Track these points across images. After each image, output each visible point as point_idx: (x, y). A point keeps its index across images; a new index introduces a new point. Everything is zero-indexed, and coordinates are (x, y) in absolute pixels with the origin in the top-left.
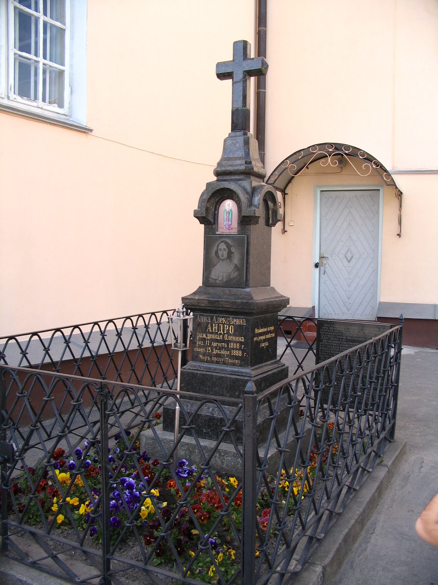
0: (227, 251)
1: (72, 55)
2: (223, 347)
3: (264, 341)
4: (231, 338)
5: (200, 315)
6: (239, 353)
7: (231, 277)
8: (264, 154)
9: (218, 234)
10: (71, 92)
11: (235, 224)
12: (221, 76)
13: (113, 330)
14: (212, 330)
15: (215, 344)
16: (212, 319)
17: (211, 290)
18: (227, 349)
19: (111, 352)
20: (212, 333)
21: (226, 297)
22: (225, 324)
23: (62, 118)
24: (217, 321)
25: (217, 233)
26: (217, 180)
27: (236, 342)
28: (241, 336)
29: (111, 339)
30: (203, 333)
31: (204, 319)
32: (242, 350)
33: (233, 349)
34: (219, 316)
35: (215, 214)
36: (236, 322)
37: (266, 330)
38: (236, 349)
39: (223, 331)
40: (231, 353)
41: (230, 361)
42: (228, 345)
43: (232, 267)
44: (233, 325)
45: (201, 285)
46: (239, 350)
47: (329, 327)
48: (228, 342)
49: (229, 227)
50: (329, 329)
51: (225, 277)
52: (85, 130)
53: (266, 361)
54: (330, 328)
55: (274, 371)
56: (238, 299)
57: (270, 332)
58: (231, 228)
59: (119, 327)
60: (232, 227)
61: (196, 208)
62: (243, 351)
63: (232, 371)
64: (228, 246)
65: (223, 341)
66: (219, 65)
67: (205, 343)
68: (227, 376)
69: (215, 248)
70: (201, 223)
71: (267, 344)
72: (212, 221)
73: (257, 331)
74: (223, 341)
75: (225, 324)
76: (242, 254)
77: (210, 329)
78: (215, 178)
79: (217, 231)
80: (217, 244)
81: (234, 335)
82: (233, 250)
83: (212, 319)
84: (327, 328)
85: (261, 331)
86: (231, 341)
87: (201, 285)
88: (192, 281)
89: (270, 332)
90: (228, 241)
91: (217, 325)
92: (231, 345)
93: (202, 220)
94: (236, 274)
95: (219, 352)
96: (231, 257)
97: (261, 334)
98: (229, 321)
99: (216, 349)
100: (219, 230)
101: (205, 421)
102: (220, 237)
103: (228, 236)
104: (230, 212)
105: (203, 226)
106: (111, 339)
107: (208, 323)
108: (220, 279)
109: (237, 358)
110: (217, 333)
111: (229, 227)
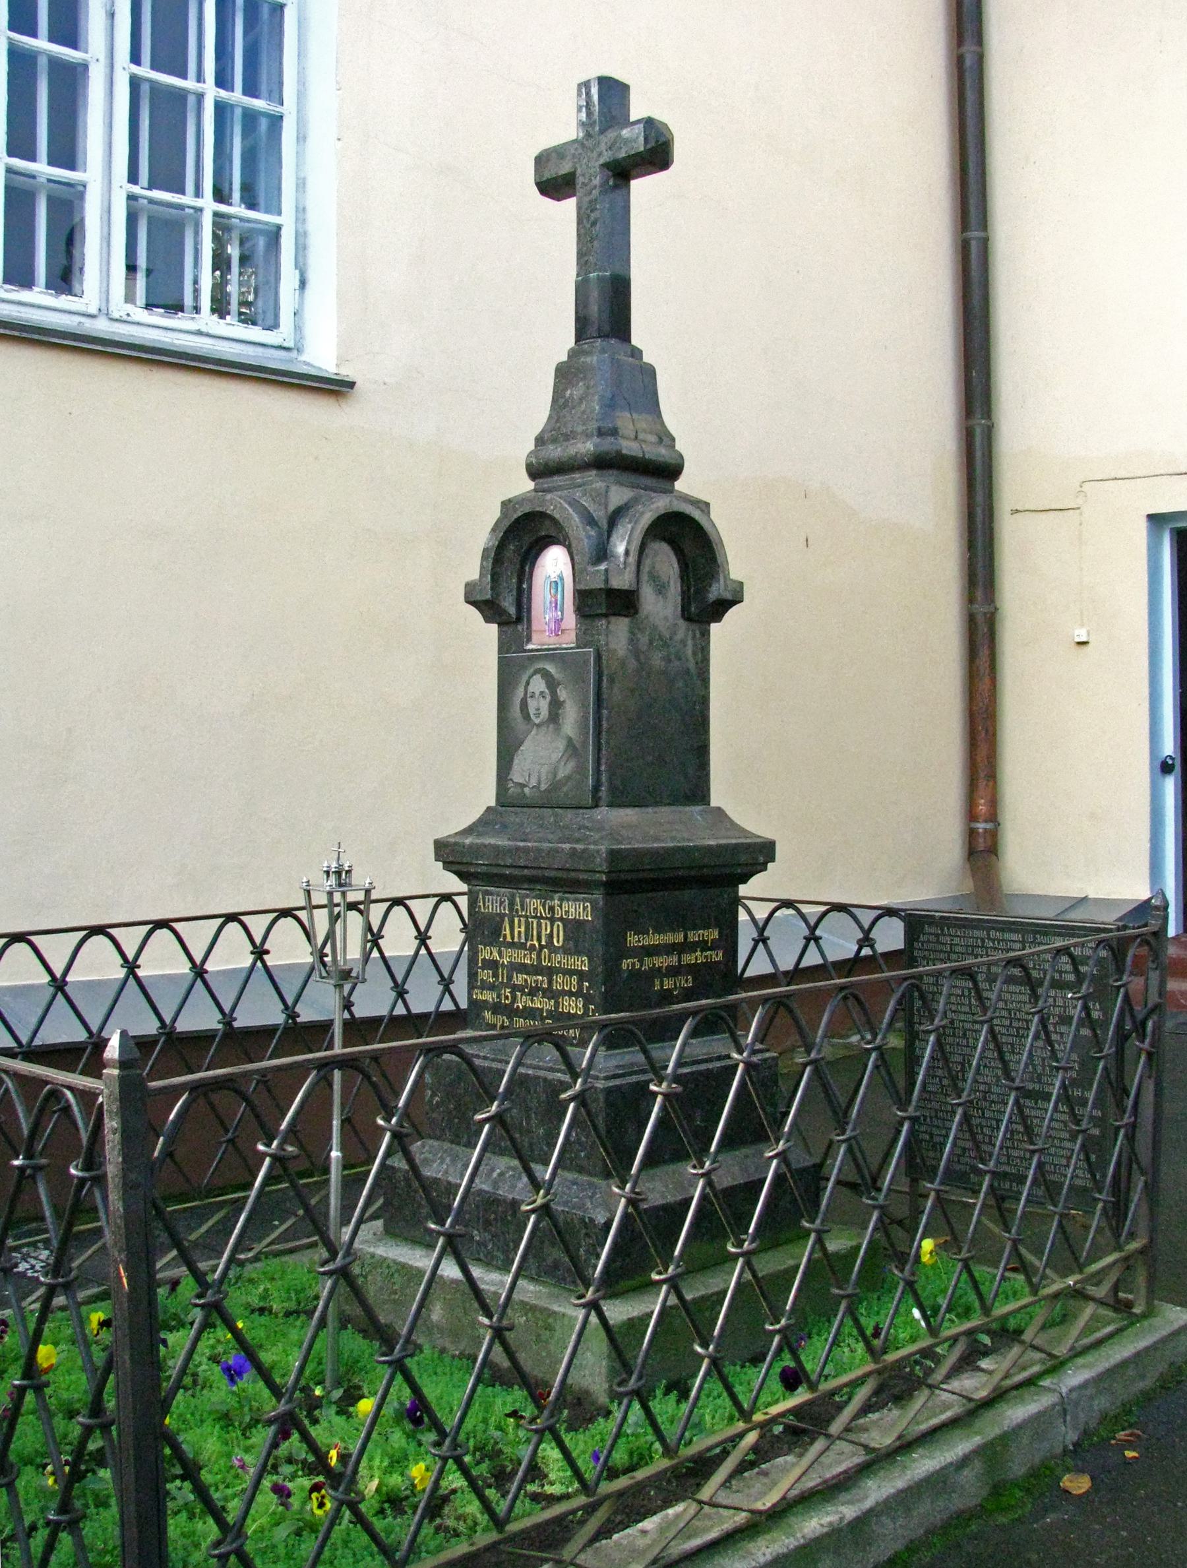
0: (548, 698)
1: (301, 185)
2: (538, 989)
3: (674, 971)
4: (559, 960)
7: (561, 775)
10: (303, 283)
11: (570, 620)
12: (554, 186)
14: (513, 938)
15: (519, 979)
16: (512, 904)
17: (513, 817)
18: (550, 993)
20: (512, 945)
21: (543, 839)
22: (542, 917)
23: (275, 360)
24: (523, 910)
25: (530, 647)
26: (535, 490)
27: (571, 973)
28: (578, 953)
30: (491, 945)
31: (494, 903)
33: (564, 993)
34: (527, 896)
35: (520, 591)
36: (567, 912)
37: (679, 938)
38: (570, 994)
39: (539, 939)
40: (557, 1003)
42: (550, 982)
43: (561, 745)
44: (561, 919)
45: (493, 803)
46: (578, 994)
47: (937, 935)
48: (550, 972)
49: (558, 629)
50: (938, 942)
51: (543, 777)
52: (336, 388)
54: (941, 939)
55: (710, 1066)
56: (568, 840)
57: (703, 945)
58: (563, 631)
61: (475, 575)
62: (588, 999)
64: (552, 684)
65: (537, 970)
66: (541, 160)
67: (495, 975)
68: (541, 1073)
69: (520, 692)
72: (512, 610)
74: (537, 970)
75: (542, 917)
76: (584, 706)
77: (508, 932)
78: (530, 485)
79: (529, 639)
80: (525, 678)
81: (566, 951)
82: (562, 694)
83: (512, 904)
84: (932, 938)
87: (493, 803)
89: (703, 945)
90: (551, 668)
93: (489, 608)
94: (571, 765)
95: (529, 1004)
96: (557, 715)
97: (651, 951)
98: (552, 909)
99: (523, 993)
100: (535, 637)
101: (477, 1207)
102: (538, 658)
103: (551, 655)
105: (495, 627)
107: (502, 916)
108: (533, 783)
110: (522, 946)
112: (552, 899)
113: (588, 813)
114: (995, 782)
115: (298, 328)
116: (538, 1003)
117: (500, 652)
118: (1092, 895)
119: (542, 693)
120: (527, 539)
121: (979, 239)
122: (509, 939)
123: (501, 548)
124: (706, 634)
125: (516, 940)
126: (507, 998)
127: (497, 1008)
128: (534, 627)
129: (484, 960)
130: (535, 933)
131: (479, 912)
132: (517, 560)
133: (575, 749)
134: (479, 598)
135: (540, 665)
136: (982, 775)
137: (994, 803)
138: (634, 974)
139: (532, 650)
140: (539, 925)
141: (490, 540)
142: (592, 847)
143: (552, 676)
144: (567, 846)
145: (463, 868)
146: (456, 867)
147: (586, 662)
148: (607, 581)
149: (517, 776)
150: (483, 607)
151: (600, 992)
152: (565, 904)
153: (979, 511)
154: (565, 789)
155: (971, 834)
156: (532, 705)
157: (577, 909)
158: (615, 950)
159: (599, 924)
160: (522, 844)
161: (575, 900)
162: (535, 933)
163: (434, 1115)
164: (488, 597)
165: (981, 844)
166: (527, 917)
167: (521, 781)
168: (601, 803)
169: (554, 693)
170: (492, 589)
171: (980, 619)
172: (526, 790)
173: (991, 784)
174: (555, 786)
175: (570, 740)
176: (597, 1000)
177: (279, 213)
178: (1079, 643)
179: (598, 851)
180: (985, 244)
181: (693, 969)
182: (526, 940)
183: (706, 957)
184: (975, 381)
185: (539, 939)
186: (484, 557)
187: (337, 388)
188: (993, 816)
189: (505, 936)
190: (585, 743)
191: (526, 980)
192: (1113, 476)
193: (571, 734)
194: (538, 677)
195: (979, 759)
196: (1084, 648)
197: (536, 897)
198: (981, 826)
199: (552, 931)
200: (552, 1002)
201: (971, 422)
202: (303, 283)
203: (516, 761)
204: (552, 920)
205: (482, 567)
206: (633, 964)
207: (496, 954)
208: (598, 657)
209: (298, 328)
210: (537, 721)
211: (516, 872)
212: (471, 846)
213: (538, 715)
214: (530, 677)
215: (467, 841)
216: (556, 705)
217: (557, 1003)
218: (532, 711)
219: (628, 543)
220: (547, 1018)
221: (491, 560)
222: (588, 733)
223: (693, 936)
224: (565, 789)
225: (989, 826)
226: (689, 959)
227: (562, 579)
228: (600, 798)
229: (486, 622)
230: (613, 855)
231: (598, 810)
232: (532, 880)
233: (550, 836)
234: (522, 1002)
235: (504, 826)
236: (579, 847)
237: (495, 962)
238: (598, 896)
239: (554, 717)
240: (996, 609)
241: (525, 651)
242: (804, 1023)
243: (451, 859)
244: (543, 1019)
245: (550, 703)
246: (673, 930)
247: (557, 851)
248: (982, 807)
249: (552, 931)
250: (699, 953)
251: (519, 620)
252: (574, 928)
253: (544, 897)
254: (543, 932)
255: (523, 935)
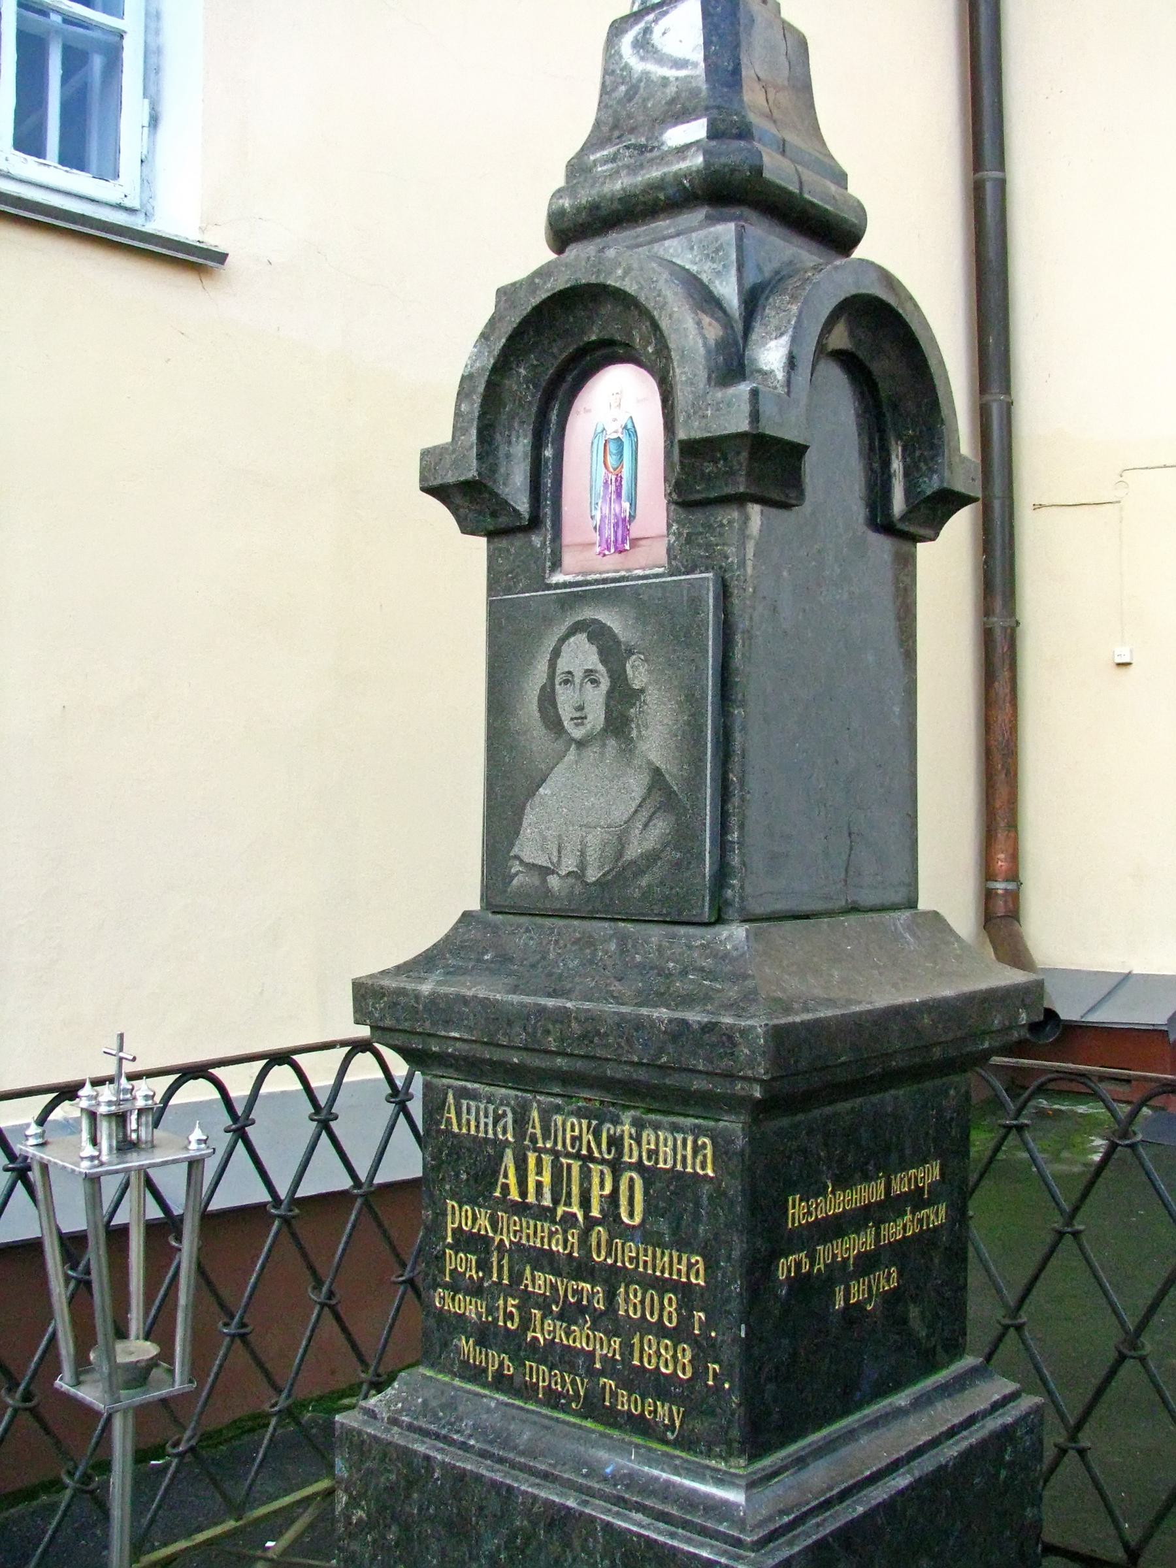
0: (605, 684)
3: (867, 1263)
4: (629, 1253)
5: (462, 1094)
6: (669, 1359)
7: (633, 851)
8: (1010, 404)
9: (557, 586)
10: (154, 121)
11: (653, 512)
13: (379, 1080)
14: (523, 1194)
15: (540, 1282)
16: (521, 1121)
17: (522, 937)
18: (607, 1320)
19: (283, 1193)
20: (521, 1209)
21: (600, 986)
22: (590, 1158)
24: (546, 1137)
25: (558, 578)
27: (662, 1286)
28: (683, 1244)
29: (282, 1139)
30: (473, 1202)
31: (477, 1116)
32: (695, 1343)
33: (643, 1327)
34: (558, 1109)
38: (661, 1331)
39: (585, 1203)
40: (627, 1348)
41: (625, 1403)
42: (611, 1297)
43: (636, 784)
44: (639, 1167)
46: (678, 1335)
48: (612, 1278)
49: (622, 537)
51: (592, 856)
52: (195, 260)
53: (883, 1389)
56: (661, 999)
57: (917, 1199)
58: (635, 542)
59: (322, 1081)
60: (635, 531)
61: (444, 436)
62: (704, 1350)
63: (631, 1480)
64: (612, 651)
65: (583, 1269)
67: (483, 1265)
69: (541, 668)
70: (467, 528)
71: (887, 1280)
72: (523, 505)
73: (799, 1212)
76: (691, 699)
77: (512, 1181)
79: (556, 564)
81: (647, 1236)
82: (638, 674)
83: (521, 1121)
85: (836, 1203)
86: (630, 1277)
87: (475, 904)
88: (417, 889)
89: (917, 1199)
90: (611, 618)
91: (547, 1159)
92: (631, 1302)
93: (468, 497)
94: (661, 827)
95: (561, 1337)
97: (834, 1228)
98: (615, 1142)
99: (547, 1313)
100: (568, 559)
103: (609, 593)
104: (621, 444)
106: (282, 1139)
108: (569, 864)
109: (658, 1386)
110: (546, 1214)
111: (622, 537)
112: (616, 1121)
113: (708, 933)
114: (1016, 831)
115: (146, 182)
116: (581, 1338)
117: (492, 588)
118: (1138, 967)
119: (589, 672)
120: (561, 351)
121: (996, 179)
122: (514, 1195)
123: (502, 366)
124: (906, 563)
125: (531, 1199)
126: (509, 1316)
127: (484, 1336)
128: (568, 537)
129: (458, 1231)
130: (575, 1190)
131: (448, 1132)
132: (532, 398)
133: (669, 793)
134: (451, 478)
135: (588, 613)
136: (1002, 824)
137: (1014, 857)
138: (801, 1283)
139: (565, 585)
140: (586, 1175)
141: (477, 356)
142: (727, 1020)
143: (614, 637)
144: (662, 1013)
145: (416, 1044)
146: (400, 1040)
147: (696, 603)
148: (755, 416)
149: (530, 847)
150: (458, 500)
151: (736, 1339)
152: (648, 1135)
153: (997, 504)
154: (644, 882)
155: (988, 896)
156: (566, 700)
157: (679, 1148)
158: (769, 1235)
159: (734, 1187)
160: (550, 1003)
161: (675, 1128)
162: (575, 1190)
163: (355, 1546)
164: (471, 473)
165: (1000, 908)
166: (556, 1154)
167: (542, 861)
168: (731, 913)
169: (618, 679)
170: (480, 457)
171: (998, 633)
172: (553, 881)
173: (1012, 834)
174: (621, 874)
175: (657, 772)
176: (730, 1353)
177: (120, 15)
178: (1119, 664)
179: (744, 1032)
180: (1002, 185)
181: (899, 1252)
182: (556, 1201)
183: (920, 1221)
184: (991, 349)
185: (585, 1203)
186: (463, 394)
187: (200, 261)
188: (1014, 876)
189: (505, 1187)
190: (694, 783)
191: (554, 1288)
192: (1162, 464)
193: (656, 758)
194: (582, 637)
195: (998, 804)
196: (1123, 670)
197: (579, 1114)
198: (1000, 886)
199: (615, 1190)
200: (616, 1343)
201: (988, 397)
202: (154, 121)
203: (529, 817)
204: (617, 1167)
205: (458, 414)
206: (798, 1265)
207: (484, 1222)
208: (724, 592)
209: (146, 182)
210: (577, 733)
211: (536, 1061)
212: (434, 998)
213: (580, 720)
214: (563, 639)
215: (426, 988)
216: (622, 697)
217: (627, 1348)
218: (566, 712)
219: (794, 340)
220: (602, 1373)
221: (477, 399)
222: (702, 759)
223: (900, 1186)
224: (644, 882)
225: (1011, 886)
226: (894, 1231)
227: (631, 430)
228: (728, 903)
229: (464, 530)
230: (778, 1034)
231: (724, 932)
232: (568, 1079)
233: (616, 987)
234: (544, 1331)
235: (504, 959)
236: (695, 1017)
237: (486, 1240)
238: (733, 1125)
239: (618, 724)
240: (1018, 623)
241: (549, 587)
242: (1168, 1394)
243: (388, 1023)
244: (591, 1373)
245: (610, 694)
246: (867, 1178)
247: (639, 1025)
248: (1001, 862)
249: (615, 1190)
250: (908, 1217)
251: (535, 522)
252: (670, 1192)
253: (597, 1116)
254: (595, 1192)
255: (547, 1191)
